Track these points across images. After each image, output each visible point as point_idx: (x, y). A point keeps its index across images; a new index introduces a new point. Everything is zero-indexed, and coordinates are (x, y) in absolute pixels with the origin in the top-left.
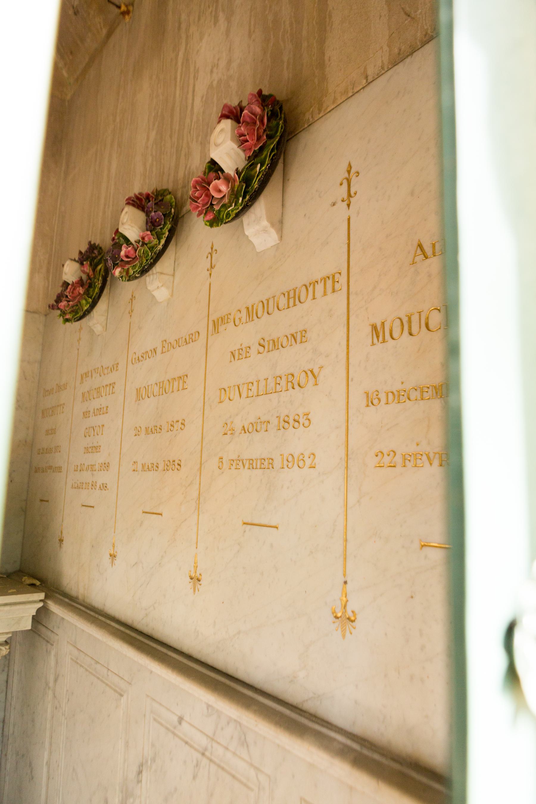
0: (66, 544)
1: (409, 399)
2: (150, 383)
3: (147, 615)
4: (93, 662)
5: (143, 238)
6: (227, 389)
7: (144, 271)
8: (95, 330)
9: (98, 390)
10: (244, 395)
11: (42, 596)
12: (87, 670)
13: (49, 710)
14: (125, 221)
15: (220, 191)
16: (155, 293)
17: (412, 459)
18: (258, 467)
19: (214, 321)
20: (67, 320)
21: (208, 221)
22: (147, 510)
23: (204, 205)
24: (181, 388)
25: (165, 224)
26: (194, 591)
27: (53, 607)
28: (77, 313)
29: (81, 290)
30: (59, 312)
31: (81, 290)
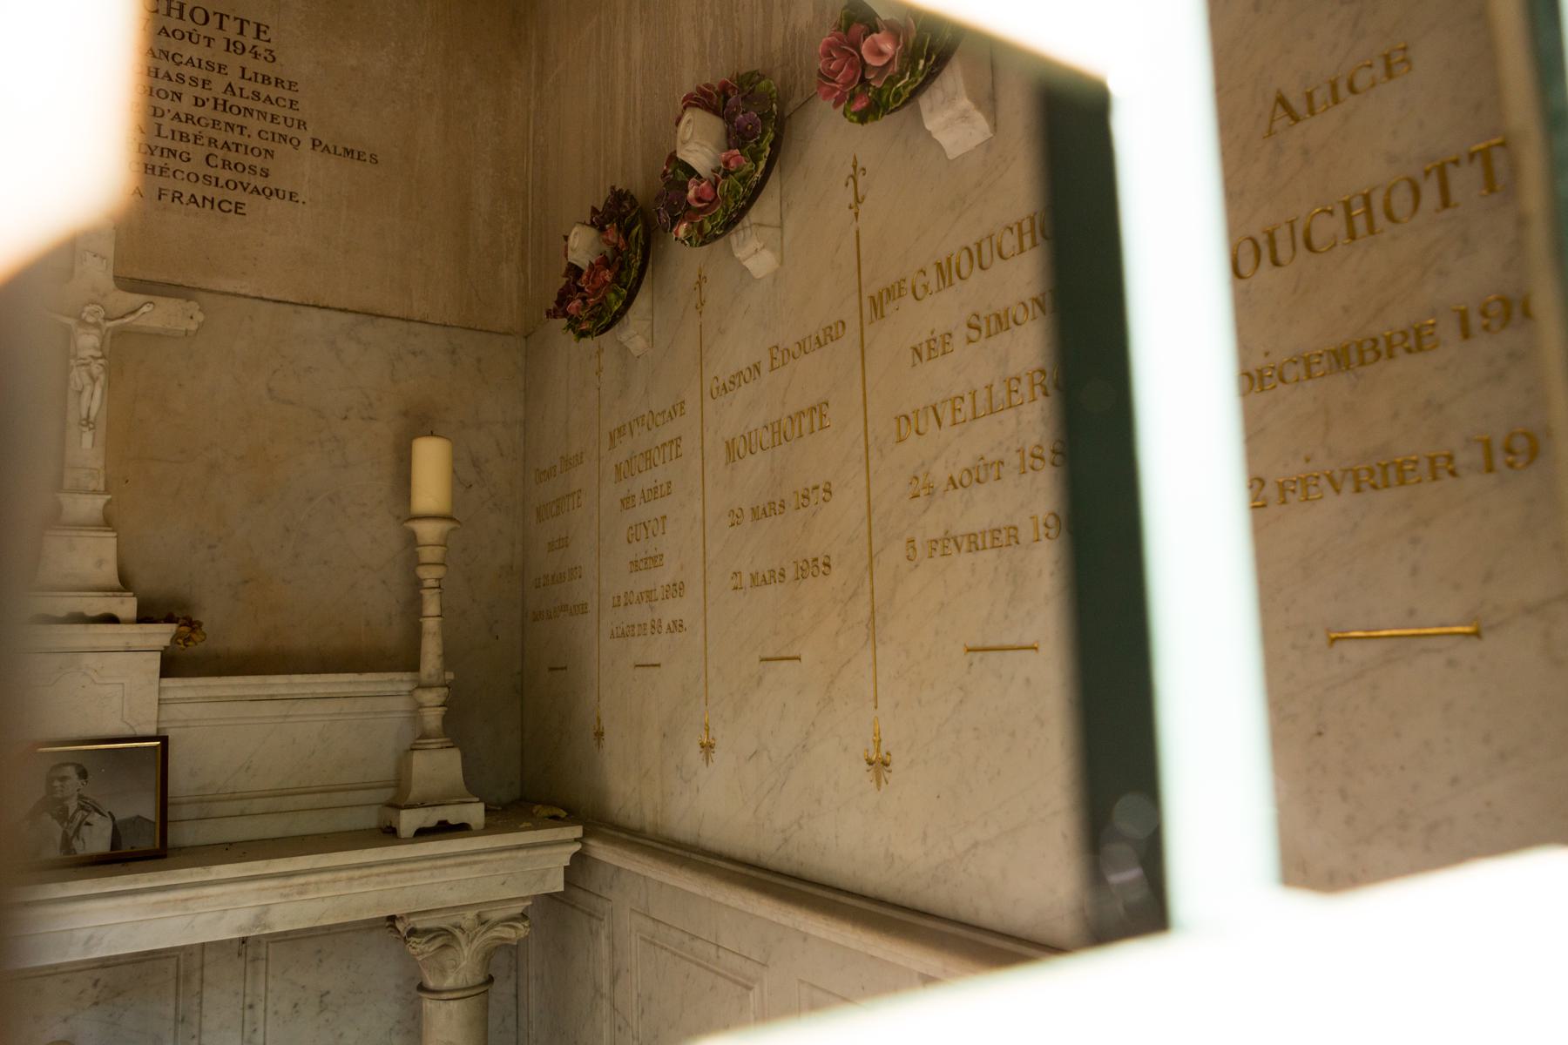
0: (612, 741)
1: (1283, 380)
2: (752, 428)
3: (786, 840)
4: (686, 938)
5: (727, 163)
6: (912, 417)
7: (730, 224)
8: (631, 347)
9: (647, 456)
10: (947, 420)
11: (577, 831)
12: (675, 954)
13: (606, 1034)
14: (688, 136)
15: (881, 53)
16: (749, 264)
17: (1298, 487)
18: (988, 544)
19: (872, 298)
20: (583, 334)
21: (854, 113)
22: (770, 654)
23: (845, 85)
24: (816, 426)
25: (764, 132)
26: (879, 785)
27: (601, 851)
28: (600, 318)
29: (608, 276)
30: (564, 322)
31: (608, 276)
